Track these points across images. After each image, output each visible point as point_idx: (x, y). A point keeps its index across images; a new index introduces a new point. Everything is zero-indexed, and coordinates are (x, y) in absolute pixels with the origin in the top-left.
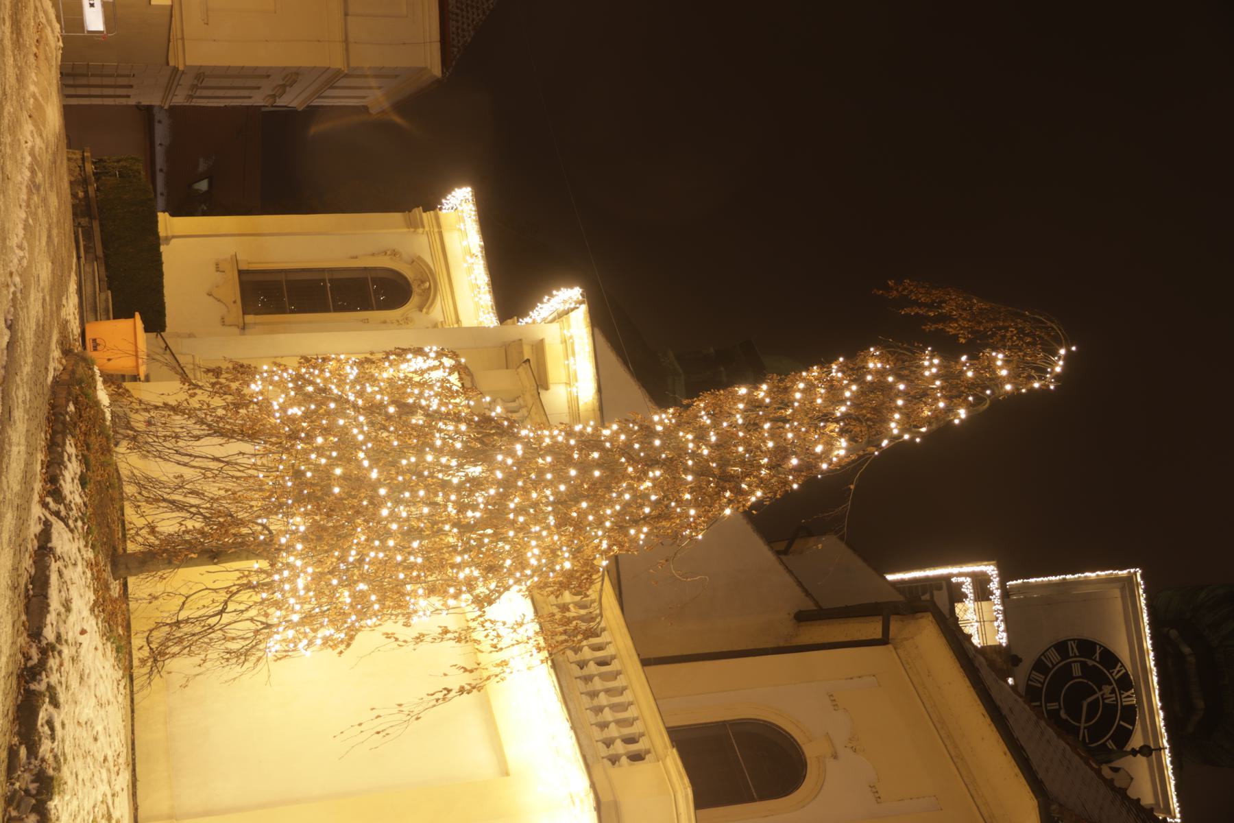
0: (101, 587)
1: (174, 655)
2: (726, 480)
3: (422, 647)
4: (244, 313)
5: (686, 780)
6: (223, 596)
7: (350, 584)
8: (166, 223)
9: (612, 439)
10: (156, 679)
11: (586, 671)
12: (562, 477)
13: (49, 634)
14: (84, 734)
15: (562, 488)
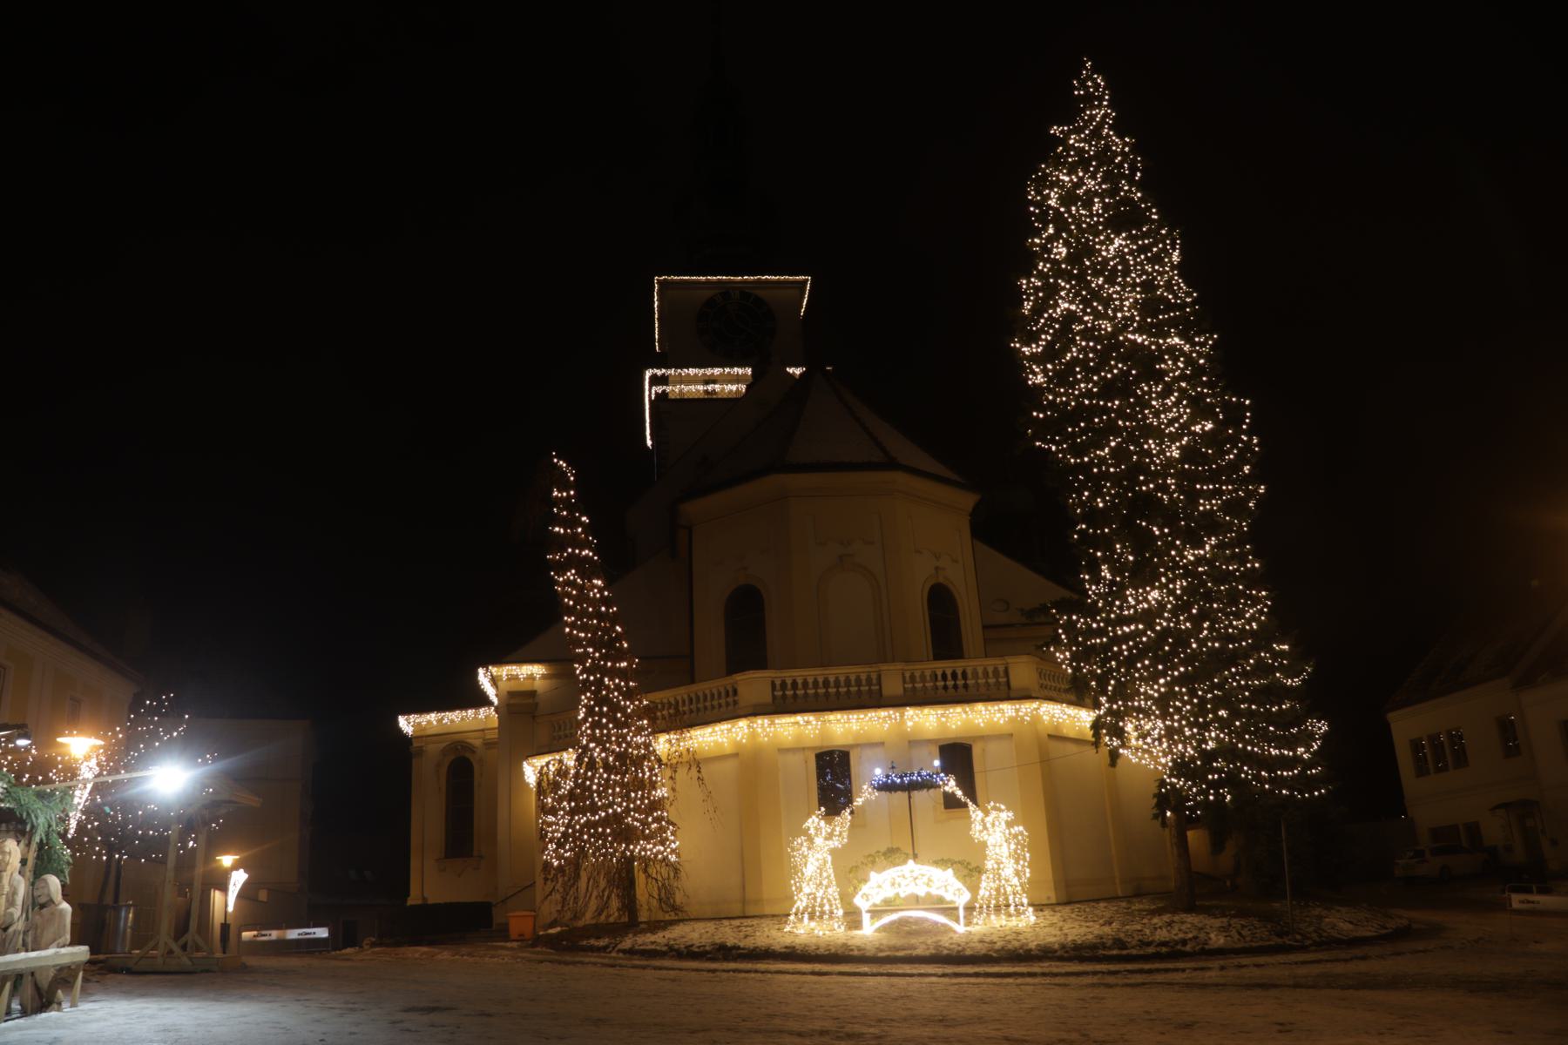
0: (643, 932)
1: (674, 901)
2: (610, 644)
3: (678, 788)
4: (472, 856)
5: (747, 672)
6: (650, 880)
7: (648, 825)
8: (414, 899)
9: (589, 699)
10: (685, 909)
11: (695, 709)
12: (606, 726)
13: (665, 949)
14: (704, 936)
15: (611, 726)
